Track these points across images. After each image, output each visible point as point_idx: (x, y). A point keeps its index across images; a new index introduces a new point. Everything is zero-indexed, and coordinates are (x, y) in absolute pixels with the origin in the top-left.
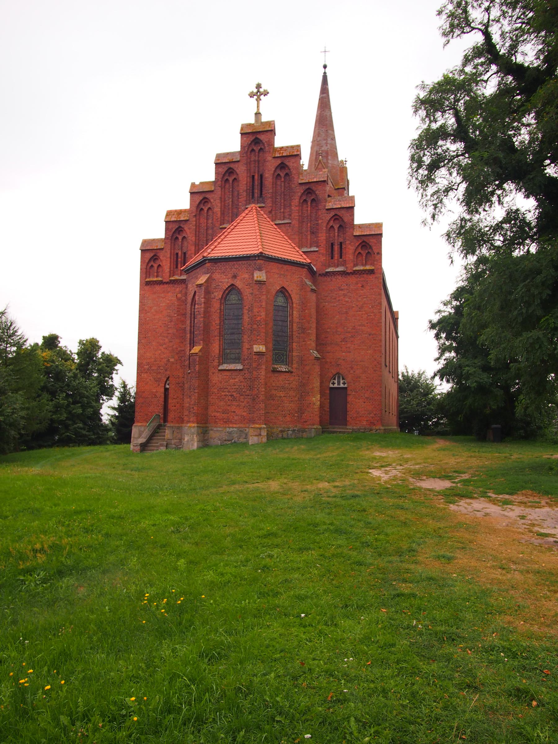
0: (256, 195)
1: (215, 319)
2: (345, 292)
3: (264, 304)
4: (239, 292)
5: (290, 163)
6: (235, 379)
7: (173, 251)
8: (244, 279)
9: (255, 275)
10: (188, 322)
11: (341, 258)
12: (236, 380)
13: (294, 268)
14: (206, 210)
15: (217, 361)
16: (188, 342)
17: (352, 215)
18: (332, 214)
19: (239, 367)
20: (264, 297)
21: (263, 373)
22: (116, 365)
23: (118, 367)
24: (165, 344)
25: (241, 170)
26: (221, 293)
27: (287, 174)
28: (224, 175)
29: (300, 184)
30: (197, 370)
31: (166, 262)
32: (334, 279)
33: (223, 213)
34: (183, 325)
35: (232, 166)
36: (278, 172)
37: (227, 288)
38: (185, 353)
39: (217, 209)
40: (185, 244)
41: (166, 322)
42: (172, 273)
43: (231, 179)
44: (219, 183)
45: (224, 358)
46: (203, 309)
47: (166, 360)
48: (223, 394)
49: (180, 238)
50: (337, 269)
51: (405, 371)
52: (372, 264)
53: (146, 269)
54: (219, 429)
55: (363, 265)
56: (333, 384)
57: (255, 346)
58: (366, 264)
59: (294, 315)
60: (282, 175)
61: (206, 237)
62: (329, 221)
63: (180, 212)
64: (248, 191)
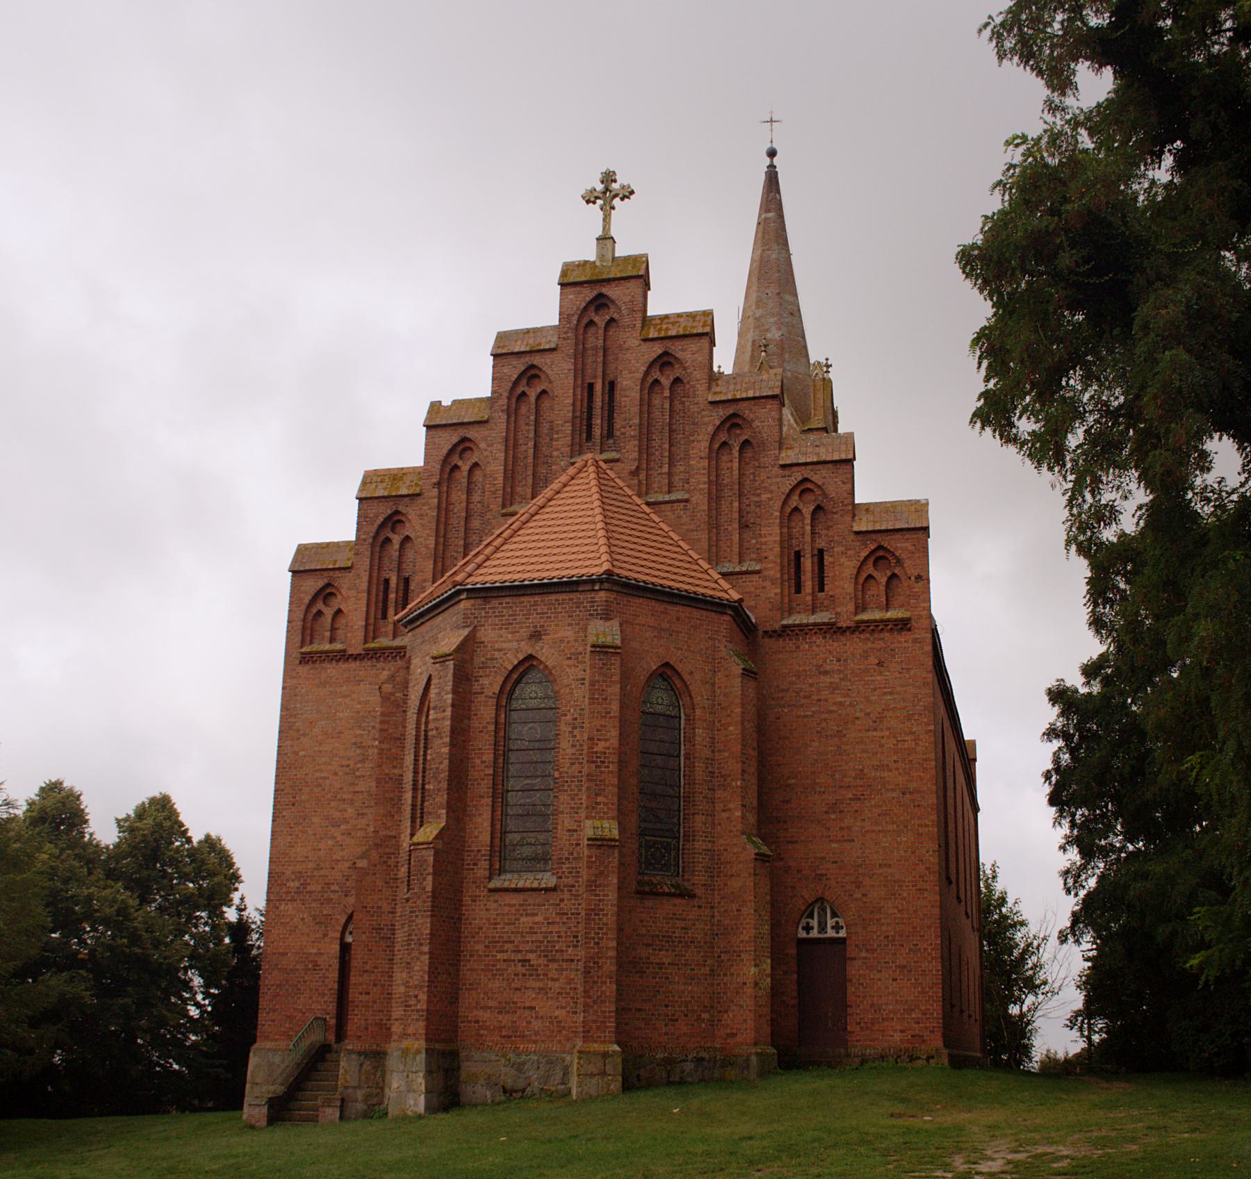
0: (597, 432)
2: (836, 678)
5: (687, 353)
7: (375, 574)
10: (409, 760)
12: (537, 919)
13: (696, 613)
14: (465, 468)
18: (797, 476)
19: (548, 880)
21: (613, 896)
24: (345, 821)
25: (560, 372)
28: (516, 383)
29: (711, 403)
31: (353, 603)
33: (510, 476)
34: (395, 767)
35: (537, 360)
37: (515, 667)
38: (398, 847)
39: (495, 467)
41: (351, 762)
43: (533, 394)
44: (501, 402)
47: (347, 864)
48: (499, 956)
53: (304, 620)
56: (808, 928)
57: (589, 823)
58: (887, 607)
62: (789, 496)
63: (396, 476)
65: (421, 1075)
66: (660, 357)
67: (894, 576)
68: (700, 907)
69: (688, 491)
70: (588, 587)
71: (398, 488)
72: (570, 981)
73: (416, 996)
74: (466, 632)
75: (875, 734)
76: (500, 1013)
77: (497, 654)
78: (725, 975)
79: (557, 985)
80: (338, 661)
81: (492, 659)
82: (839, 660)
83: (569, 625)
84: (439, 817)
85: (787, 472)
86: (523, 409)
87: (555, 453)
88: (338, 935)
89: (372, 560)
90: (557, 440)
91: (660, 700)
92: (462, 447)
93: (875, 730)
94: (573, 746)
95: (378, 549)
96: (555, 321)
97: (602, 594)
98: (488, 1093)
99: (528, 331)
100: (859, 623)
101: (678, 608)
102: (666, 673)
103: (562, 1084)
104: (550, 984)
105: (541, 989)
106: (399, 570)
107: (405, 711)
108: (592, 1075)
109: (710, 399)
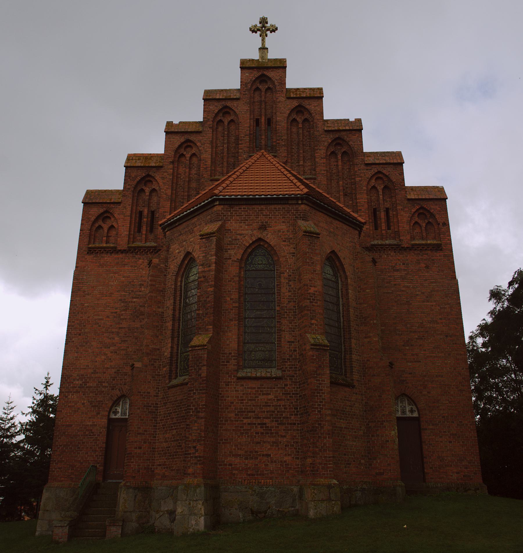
6: (268, 394)
7: (134, 208)
8: (279, 231)
11: (389, 228)
12: (270, 397)
14: (188, 156)
16: (169, 333)
18: (375, 170)
19: (275, 372)
25: (242, 110)
26: (241, 251)
27: (306, 120)
28: (217, 115)
29: (326, 131)
30: (204, 374)
31: (123, 223)
33: (213, 162)
34: (159, 307)
35: (229, 104)
36: (294, 116)
37: (250, 245)
39: (207, 156)
40: (155, 199)
41: (118, 311)
44: (208, 123)
46: (213, 273)
47: (113, 370)
48: (245, 421)
49: (147, 190)
53: (90, 230)
55: (423, 239)
59: (350, 296)
61: (188, 192)
64: (252, 136)
65: (201, 502)
66: (297, 107)
68: (356, 394)
69: (315, 174)
70: (294, 202)
71: (149, 163)
73: (195, 447)
74: (220, 223)
75: (428, 304)
76: (246, 459)
77: (238, 237)
78: (373, 436)
79: (285, 440)
80: (111, 253)
81: (236, 240)
82: (404, 264)
83: (283, 222)
84: (207, 330)
85: (369, 168)
87: (240, 151)
88: (107, 413)
89: (133, 200)
90: (241, 144)
92: (186, 145)
93: (428, 301)
94: (289, 291)
95: (136, 194)
96: (238, 87)
97: (303, 206)
98: (241, 515)
100: (413, 245)
101: (337, 222)
103: (292, 507)
104: (280, 439)
105: (273, 442)
106: (149, 207)
107: (165, 275)
108: (323, 500)
109: (325, 129)
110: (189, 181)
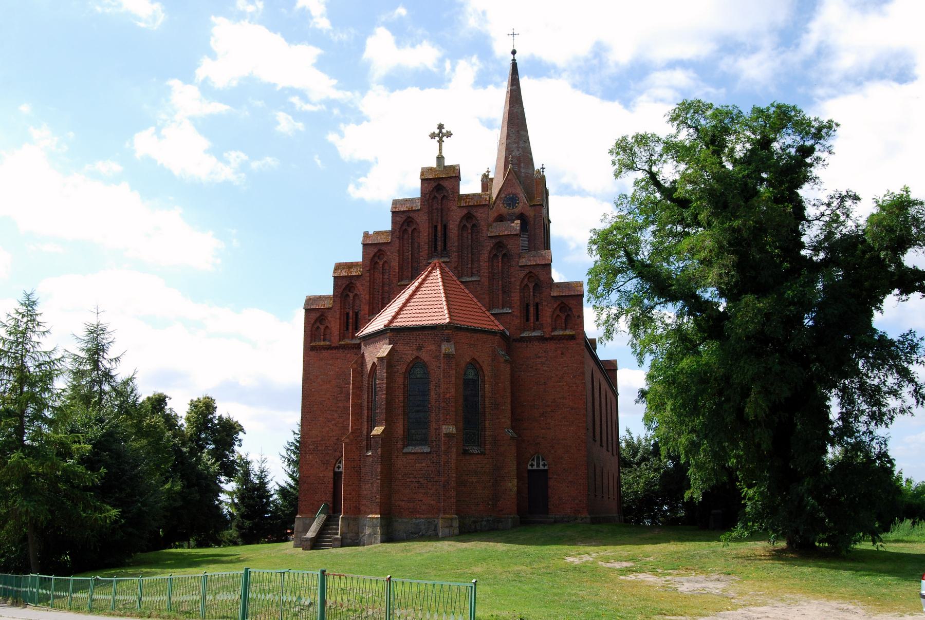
0: (439, 248)
1: (399, 396)
2: (544, 359)
3: (453, 379)
4: (424, 366)
9: (443, 347)
10: (365, 396)
13: (485, 336)
14: (381, 263)
15: (400, 443)
17: (549, 272)
19: (426, 449)
20: (454, 372)
21: (454, 457)
22: (237, 433)
23: (241, 435)
24: (334, 419)
25: (422, 221)
26: (405, 366)
27: (474, 225)
28: (402, 225)
31: (335, 326)
32: (530, 346)
33: (401, 268)
35: (411, 215)
38: (361, 432)
39: (395, 264)
40: (358, 302)
42: (342, 336)
43: (410, 230)
45: (409, 439)
50: (534, 334)
51: (628, 437)
52: (573, 328)
54: (405, 520)
56: (532, 465)
57: (444, 427)
58: (566, 329)
60: (469, 226)
62: (523, 279)
63: (350, 266)
67: (568, 315)
72: (437, 490)
86: (406, 236)
91: (471, 374)
99: (406, 200)
102: (474, 364)
106: (353, 309)
110: (383, 286)
